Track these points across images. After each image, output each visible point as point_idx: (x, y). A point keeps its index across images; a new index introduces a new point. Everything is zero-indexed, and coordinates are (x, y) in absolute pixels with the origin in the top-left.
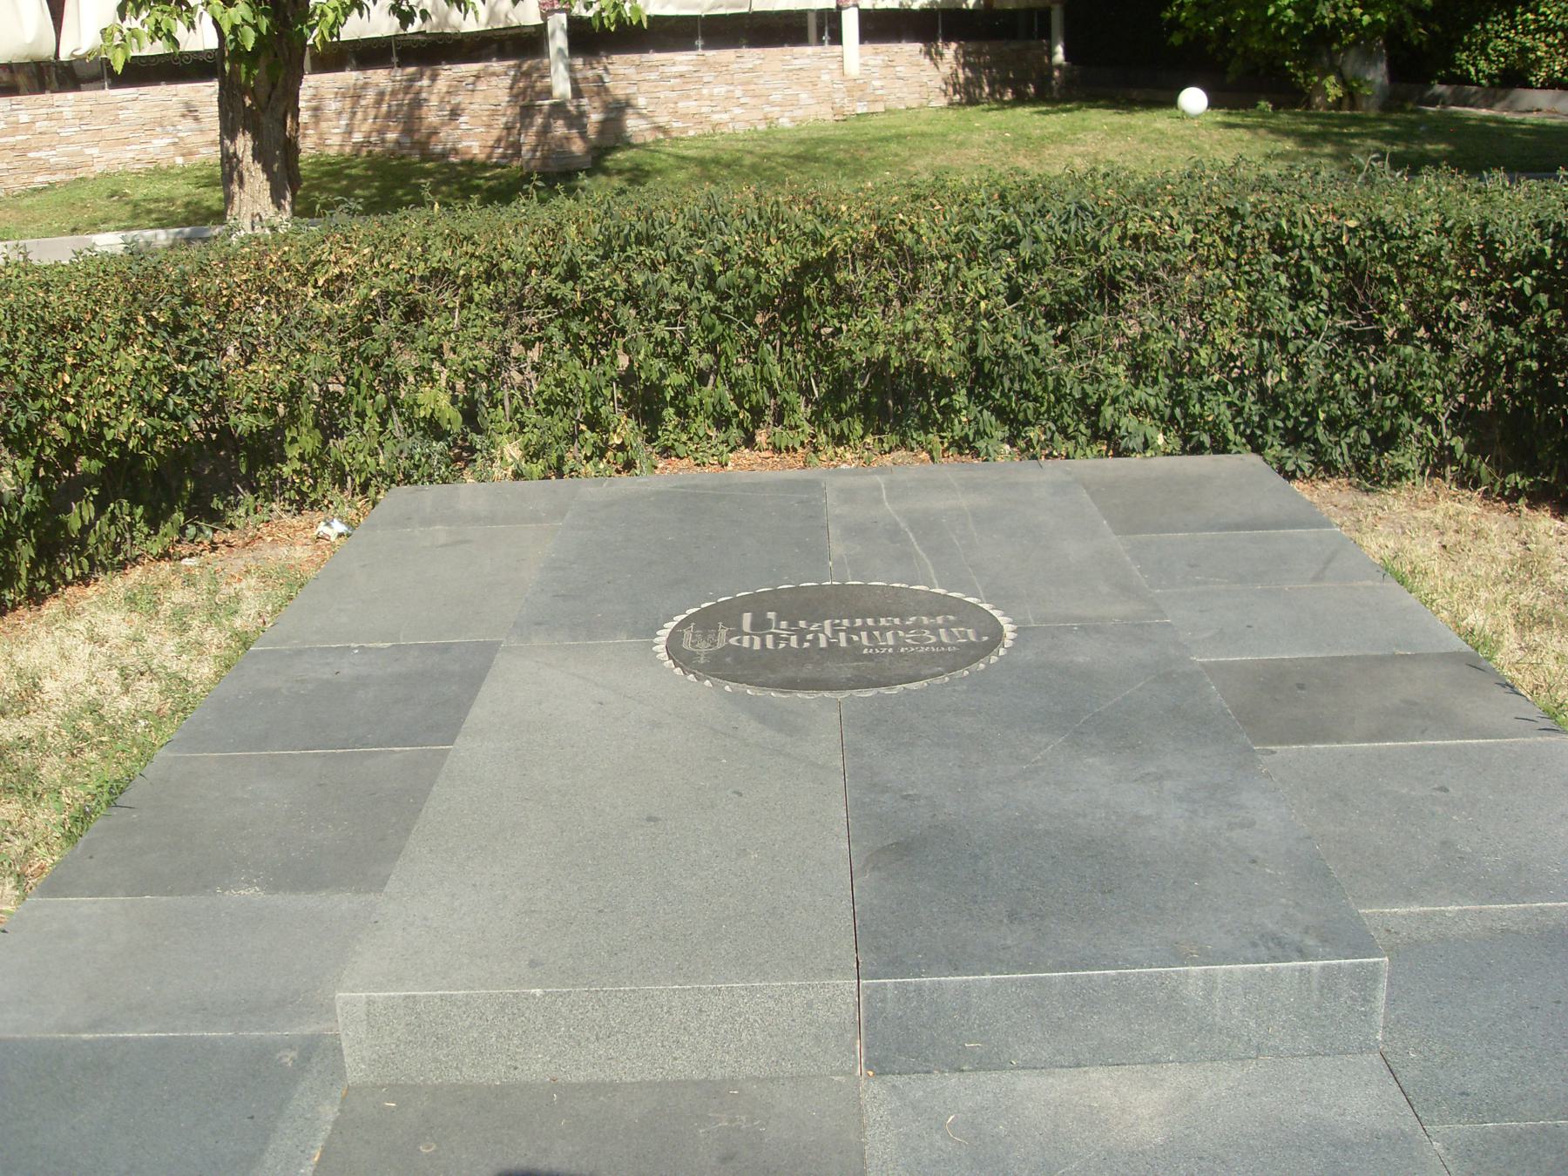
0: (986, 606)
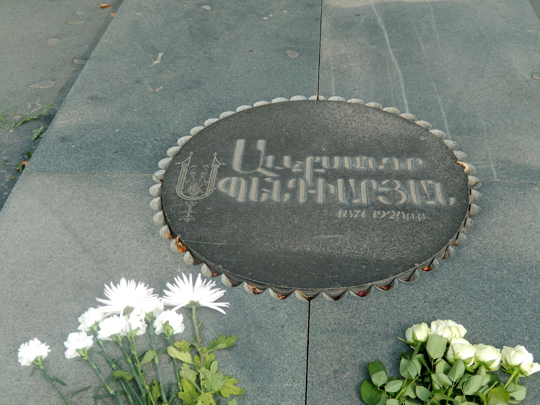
0: (449, 143)
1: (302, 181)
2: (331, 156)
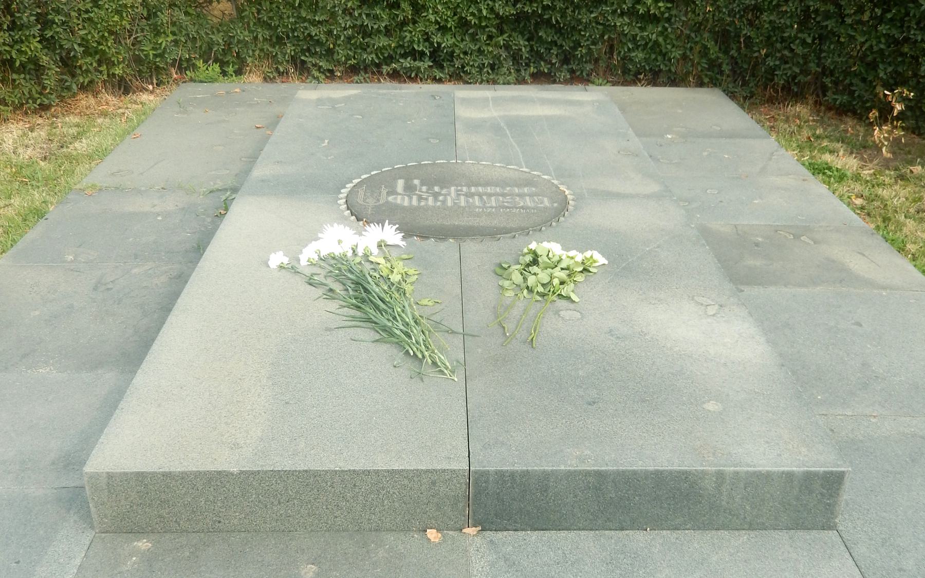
0: (556, 182)
1: (449, 198)
2: (469, 186)
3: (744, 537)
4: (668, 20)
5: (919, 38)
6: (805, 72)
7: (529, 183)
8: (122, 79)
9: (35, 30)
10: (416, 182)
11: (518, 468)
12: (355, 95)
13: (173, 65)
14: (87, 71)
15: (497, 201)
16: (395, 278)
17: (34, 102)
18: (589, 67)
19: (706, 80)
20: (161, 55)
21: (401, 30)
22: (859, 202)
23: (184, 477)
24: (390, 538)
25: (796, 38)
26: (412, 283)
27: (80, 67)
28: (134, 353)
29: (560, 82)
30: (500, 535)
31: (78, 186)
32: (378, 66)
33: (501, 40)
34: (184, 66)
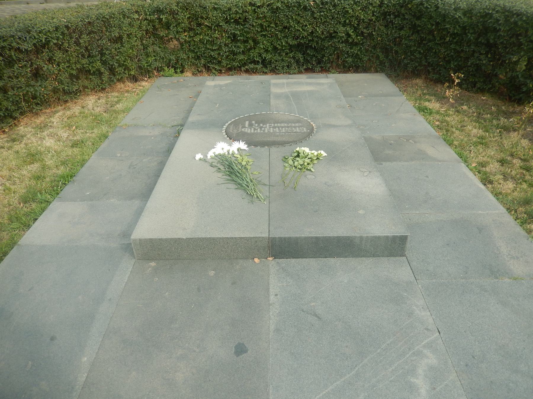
0: (309, 121)
2: (274, 123)
3: (371, 259)
4: (362, 44)
5: (468, 50)
6: (420, 65)
7: (298, 121)
8: (134, 76)
9: (98, 58)
10: (253, 122)
11: (286, 236)
12: (230, 83)
13: (155, 69)
14: (120, 73)
15: (285, 129)
16: (244, 163)
17: (99, 87)
18: (329, 65)
19: (379, 70)
20: (150, 66)
21: (249, 52)
22: (437, 123)
23: (166, 240)
24: (241, 261)
25: (416, 50)
26: (250, 165)
27: (117, 72)
28: (146, 194)
29: (317, 72)
30: (281, 260)
31: (120, 125)
32: (240, 67)
33: (291, 55)
34: (159, 70)
